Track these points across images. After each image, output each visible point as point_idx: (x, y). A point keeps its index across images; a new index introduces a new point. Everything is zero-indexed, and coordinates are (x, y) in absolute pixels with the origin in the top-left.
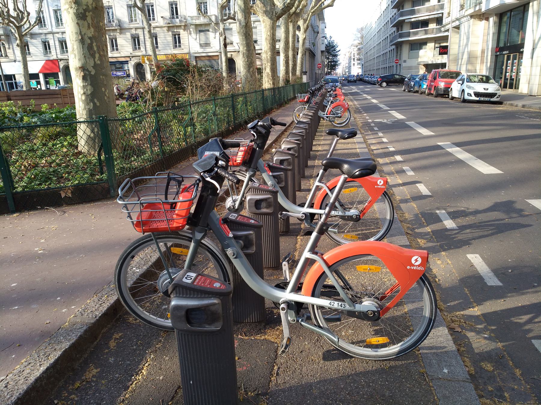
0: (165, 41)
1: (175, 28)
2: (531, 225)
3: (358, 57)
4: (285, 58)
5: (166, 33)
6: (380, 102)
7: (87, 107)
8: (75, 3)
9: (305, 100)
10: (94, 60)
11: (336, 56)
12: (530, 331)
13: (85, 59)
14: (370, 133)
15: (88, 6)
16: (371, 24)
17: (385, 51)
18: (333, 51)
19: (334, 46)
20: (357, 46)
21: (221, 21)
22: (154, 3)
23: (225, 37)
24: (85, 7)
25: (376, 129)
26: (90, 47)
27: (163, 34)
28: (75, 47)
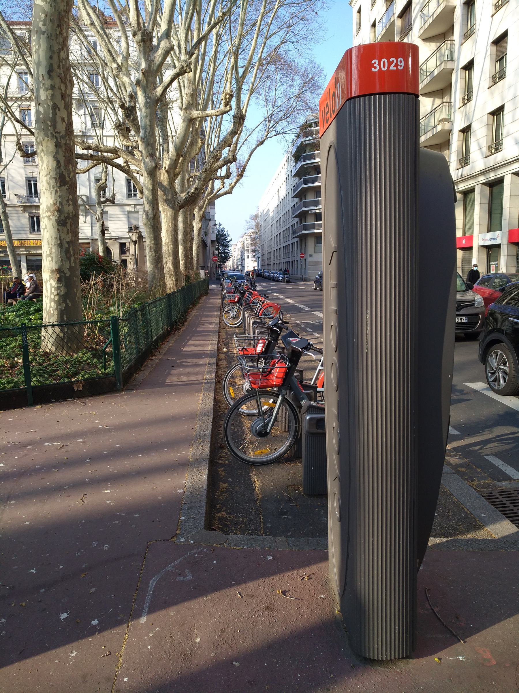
0: (19, 224)
1: (34, 208)
2: (471, 400)
3: (252, 248)
4: (184, 251)
5: (21, 215)
6: (298, 302)
7: (59, 307)
8: (57, 211)
9: (236, 300)
10: (70, 263)
11: (227, 246)
12: (482, 453)
13: (62, 262)
14: (305, 334)
15: (69, 214)
16: (268, 211)
17: (287, 243)
18: (223, 240)
19: (225, 235)
20: (251, 235)
21: (98, 204)
22: (6, 178)
23: (103, 222)
24: (66, 215)
25: (309, 330)
26: (67, 251)
27: (15, 215)
28: (53, 251)
